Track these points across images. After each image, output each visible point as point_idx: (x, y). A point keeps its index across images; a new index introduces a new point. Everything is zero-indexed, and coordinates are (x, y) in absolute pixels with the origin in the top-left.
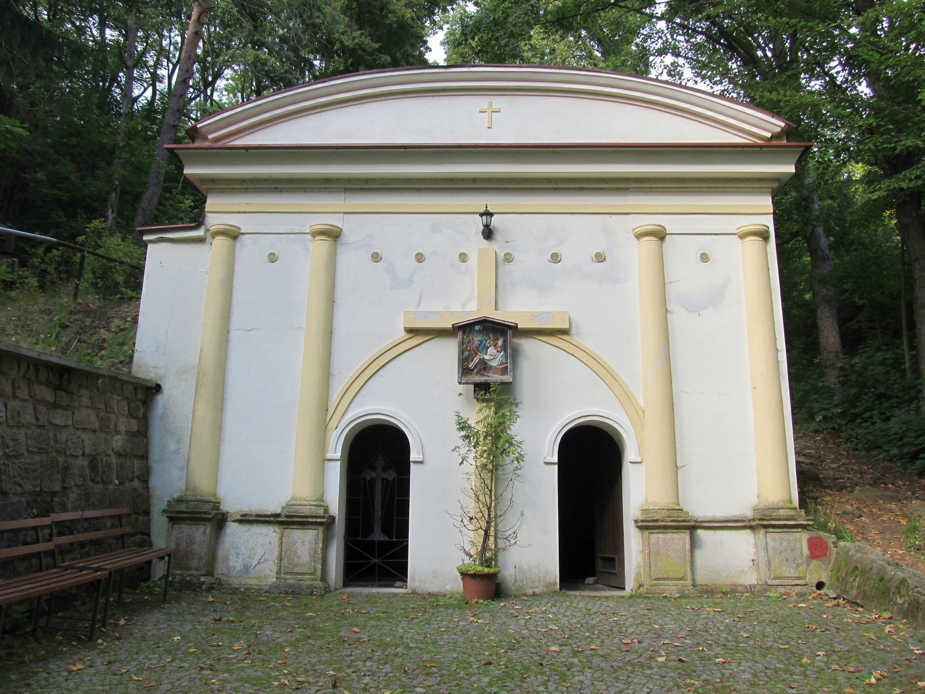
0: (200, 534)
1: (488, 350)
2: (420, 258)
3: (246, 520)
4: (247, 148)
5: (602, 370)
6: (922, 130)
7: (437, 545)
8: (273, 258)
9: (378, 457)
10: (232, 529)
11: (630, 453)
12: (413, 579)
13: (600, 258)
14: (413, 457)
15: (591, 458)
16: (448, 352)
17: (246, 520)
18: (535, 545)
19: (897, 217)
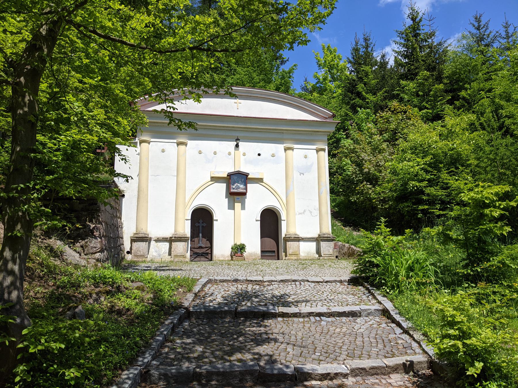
0: (143, 245)
1: (236, 185)
2: (215, 153)
3: (158, 240)
4: (324, 114)
5: (273, 192)
6: (1, 170)
7: (222, 247)
8: (163, 151)
9: (202, 221)
10: (153, 243)
11: (283, 216)
12: (215, 257)
13: (273, 156)
14: (215, 218)
15: (270, 220)
16: (223, 186)
17: (158, 240)
18: (253, 244)
19: (205, 312)
